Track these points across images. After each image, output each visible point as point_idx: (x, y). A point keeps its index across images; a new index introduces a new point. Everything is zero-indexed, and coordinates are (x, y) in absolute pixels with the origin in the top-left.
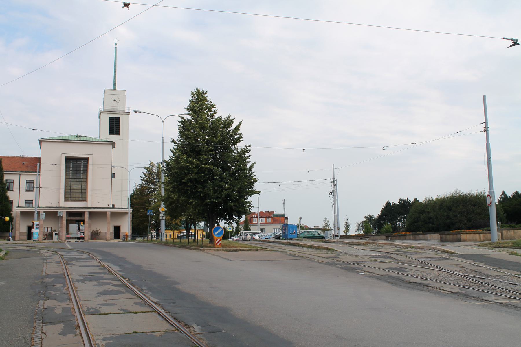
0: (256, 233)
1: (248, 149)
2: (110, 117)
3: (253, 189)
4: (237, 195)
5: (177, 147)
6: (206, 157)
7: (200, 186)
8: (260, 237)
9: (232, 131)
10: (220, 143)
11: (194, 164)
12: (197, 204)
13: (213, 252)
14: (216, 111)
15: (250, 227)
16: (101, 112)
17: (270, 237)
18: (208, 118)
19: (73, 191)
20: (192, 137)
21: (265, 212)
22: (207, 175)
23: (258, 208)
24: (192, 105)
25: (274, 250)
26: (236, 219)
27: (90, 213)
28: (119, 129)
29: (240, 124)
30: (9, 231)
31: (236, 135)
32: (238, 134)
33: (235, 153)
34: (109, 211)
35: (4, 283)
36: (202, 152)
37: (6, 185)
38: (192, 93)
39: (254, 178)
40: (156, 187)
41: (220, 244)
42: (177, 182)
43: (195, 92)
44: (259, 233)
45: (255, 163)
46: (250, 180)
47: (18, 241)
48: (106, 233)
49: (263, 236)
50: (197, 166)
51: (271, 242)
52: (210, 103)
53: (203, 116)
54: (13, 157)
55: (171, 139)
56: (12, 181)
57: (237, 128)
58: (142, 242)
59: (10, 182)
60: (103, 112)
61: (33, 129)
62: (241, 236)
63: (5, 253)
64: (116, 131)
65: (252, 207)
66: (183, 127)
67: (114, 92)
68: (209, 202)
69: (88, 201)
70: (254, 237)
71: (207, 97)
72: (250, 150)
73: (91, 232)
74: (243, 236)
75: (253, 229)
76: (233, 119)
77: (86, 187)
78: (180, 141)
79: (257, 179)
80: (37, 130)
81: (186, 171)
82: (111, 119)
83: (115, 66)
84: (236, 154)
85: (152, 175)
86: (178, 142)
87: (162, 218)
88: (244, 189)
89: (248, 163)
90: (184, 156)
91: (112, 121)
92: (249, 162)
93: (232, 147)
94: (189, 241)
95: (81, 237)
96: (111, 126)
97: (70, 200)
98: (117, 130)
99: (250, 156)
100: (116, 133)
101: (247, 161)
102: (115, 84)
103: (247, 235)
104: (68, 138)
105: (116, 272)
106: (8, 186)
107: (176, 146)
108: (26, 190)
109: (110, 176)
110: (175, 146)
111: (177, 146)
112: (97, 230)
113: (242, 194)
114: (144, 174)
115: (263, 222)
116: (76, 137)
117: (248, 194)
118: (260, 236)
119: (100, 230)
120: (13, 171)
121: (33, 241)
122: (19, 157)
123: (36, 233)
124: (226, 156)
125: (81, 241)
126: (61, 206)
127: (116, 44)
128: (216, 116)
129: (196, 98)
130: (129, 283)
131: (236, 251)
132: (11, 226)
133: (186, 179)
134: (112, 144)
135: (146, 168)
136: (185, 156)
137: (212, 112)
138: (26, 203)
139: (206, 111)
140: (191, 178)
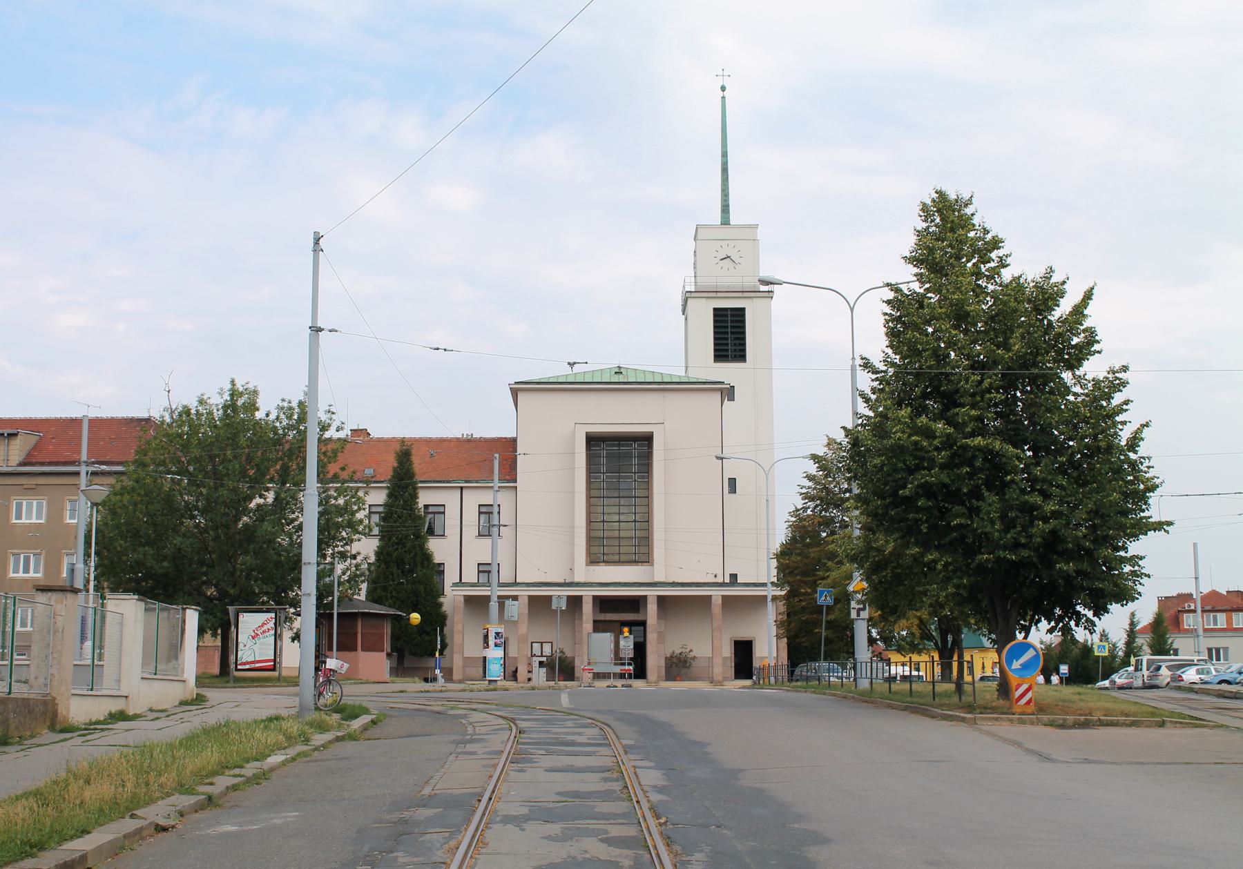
0: (1190, 664)
1: (1120, 379)
2: (715, 310)
3: (1142, 514)
4: (1085, 536)
5: (880, 384)
6: (973, 412)
7: (958, 509)
8: (1202, 676)
9: (1060, 322)
10: (1026, 362)
11: (935, 437)
12: (951, 568)
13: (1005, 728)
14: (1004, 258)
15: (1172, 643)
16: (688, 295)
17: (1238, 675)
18: (980, 282)
19: (611, 534)
20: (927, 350)
21: (1227, 592)
22: (981, 470)
23: (1196, 578)
24: (925, 243)
25: (1222, 726)
26: (1086, 615)
27: (661, 600)
28: (744, 345)
29: (1088, 296)
30: (435, 654)
31: (1077, 335)
32: (1084, 331)
33: (1076, 394)
34: (717, 594)
35: (295, 817)
36: (962, 396)
37: (425, 522)
38: (924, 208)
39: (1147, 475)
40: (847, 517)
41: (1031, 699)
42: (883, 498)
43: (933, 201)
44: (1202, 663)
45: (1147, 425)
46: (1132, 483)
47: (460, 682)
48: (710, 659)
49: (1214, 673)
50: (949, 442)
51: (1226, 694)
52: (984, 234)
53: (961, 278)
54: (442, 441)
55: (862, 359)
56: (440, 510)
57: (1079, 312)
58: (801, 691)
59: (434, 513)
60: (693, 295)
61: (436, 347)
62: (1139, 674)
63: (370, 720)
64: (735, 344)
65: (1146, 575)
66: (900, 317)
67: (725, 232)
68: (987, 560)
69: (655, 565)
70: (1180, 676)
71: (973, 215)
72: (1128, 383)
73: (666, 657)
74: (1145, 673)
75: (1184, 647)
76: (1064, 283)
77: (648, 521)
78: (893, 364)
79: (1157, 481)
80: (445, 350)
81: (912, 462)
82: (719, 314)
83: (725, 155)
84: (1079, 399)
85: (834, 479)
86: (884, 368)
87: (858, 615)
88: (1110, 516)
89: (1120, 427)
90: (903, 412)
91: (737, 321)
92: (1124, 423)
93: (1067, 376)
94: (913, 688)
95: (625, 674)
96: (742, 336)
97: (604, 562)
98: (738, 348)
99: (1127, 402)
100: (735, 356)
101: (1118, 419)
102: (725, 209)
103: (1159, 668)
104: (654, 379)
105: (645, 792)
106: (430, 523)
107: (877, 379)
108: (479, 535)
109: (716, 486)
110: (873, 380)
111: (881, 381)
112: (683, 650)
113: (1104, 533)
114: (810, 478)
115: (1219, 626)
116: (616, 373)
117: (1124, 532)
118: (1203, 673)
119: (691, 651)
120: (441, 481)
121: (487, 682)
122: (458, 439)
123: (495, 658)
124: (1042, 405)
125: (623, 686)
126: (577, 580)
127: (723, 89)
128: (1007, 275)
129: (938, 220)
130: (661, 834)
131: (1085, 725)
132: (439, 639)
133: (910, 486)
134: (721, 391)
135: (814, 457)
136: (905, 412)
137: (992, 265)
138: (479, 572)
139: (974, 261)
140: (926, 481)
